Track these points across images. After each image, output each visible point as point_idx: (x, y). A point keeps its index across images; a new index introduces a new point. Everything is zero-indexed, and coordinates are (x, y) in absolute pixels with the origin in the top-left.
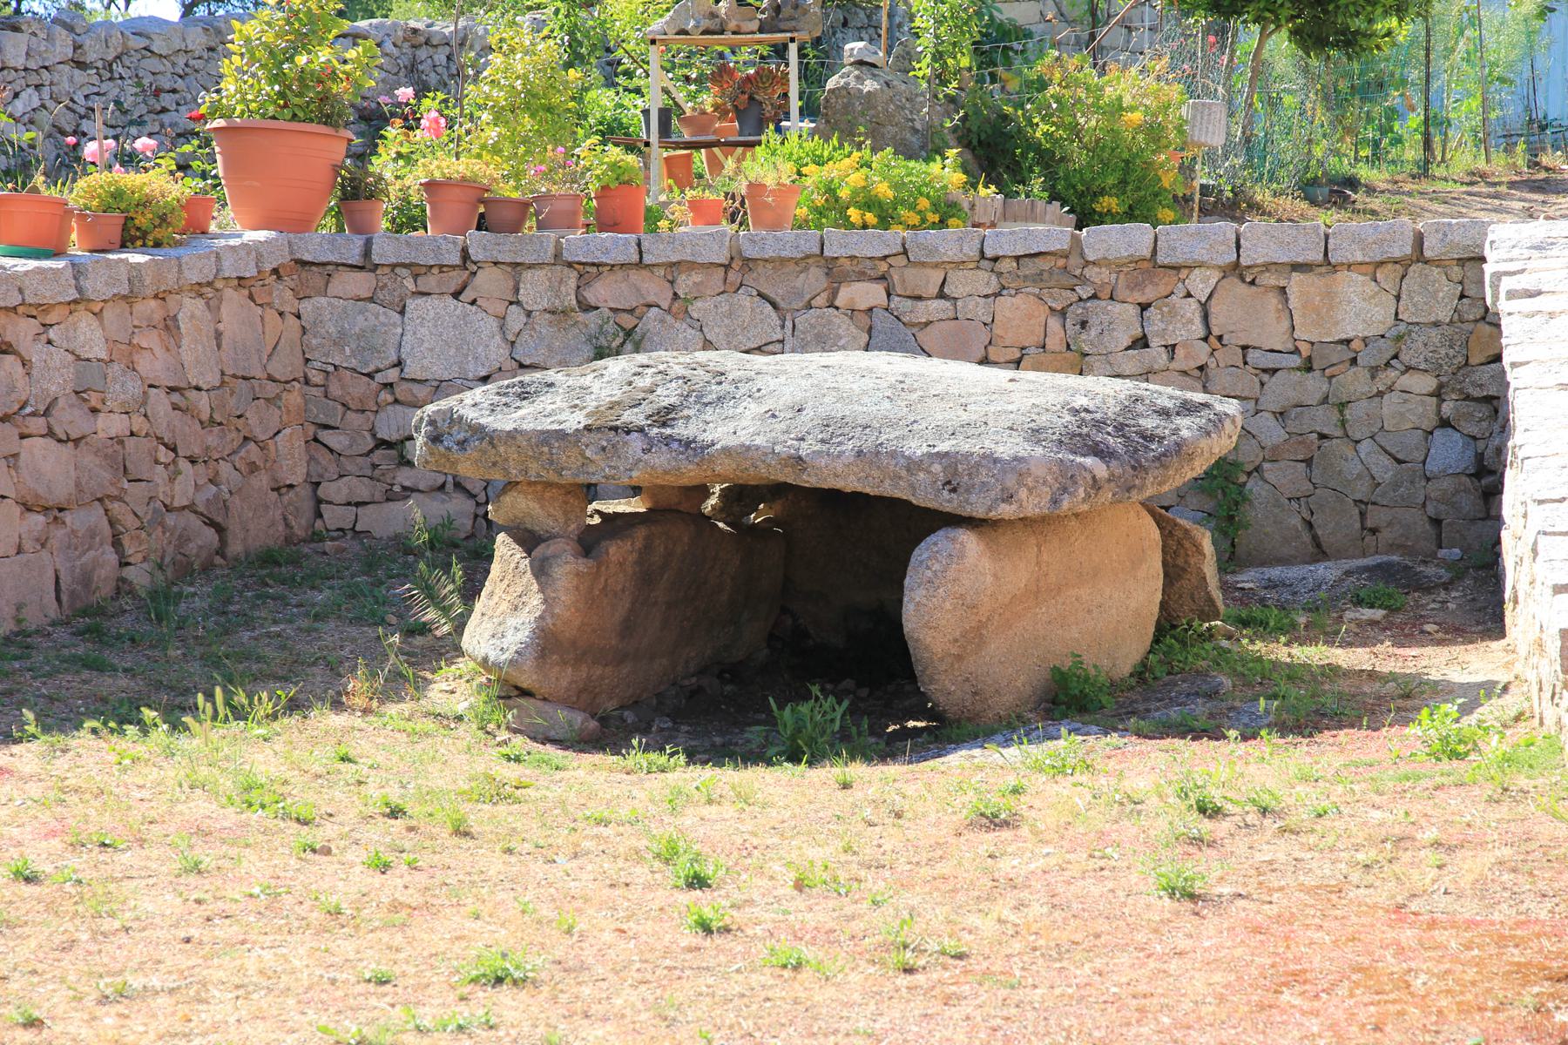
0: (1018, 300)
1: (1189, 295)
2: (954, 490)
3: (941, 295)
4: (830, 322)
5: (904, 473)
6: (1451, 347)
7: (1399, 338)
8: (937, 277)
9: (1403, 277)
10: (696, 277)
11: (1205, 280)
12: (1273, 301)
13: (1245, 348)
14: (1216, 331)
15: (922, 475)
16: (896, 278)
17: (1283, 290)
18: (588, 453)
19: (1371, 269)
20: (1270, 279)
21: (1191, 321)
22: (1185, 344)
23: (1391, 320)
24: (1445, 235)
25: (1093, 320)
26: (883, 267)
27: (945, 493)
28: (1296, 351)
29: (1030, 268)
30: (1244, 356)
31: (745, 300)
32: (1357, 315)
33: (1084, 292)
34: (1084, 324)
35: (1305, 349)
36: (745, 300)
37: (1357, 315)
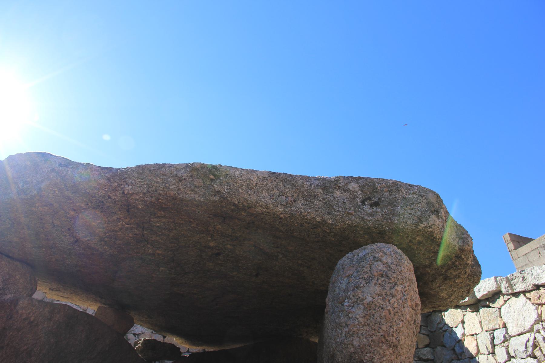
2: (376, 204)
5: (319, 191)
15: (338, 193)
27: (367, 208)
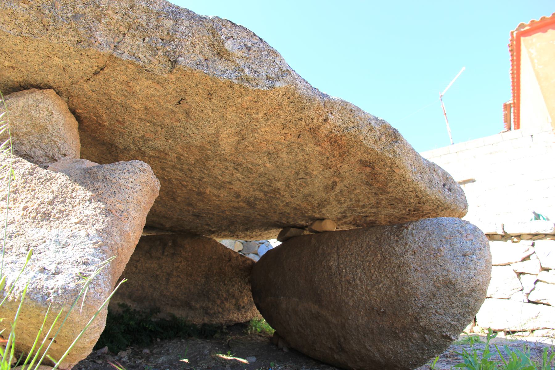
18: (229, 45)
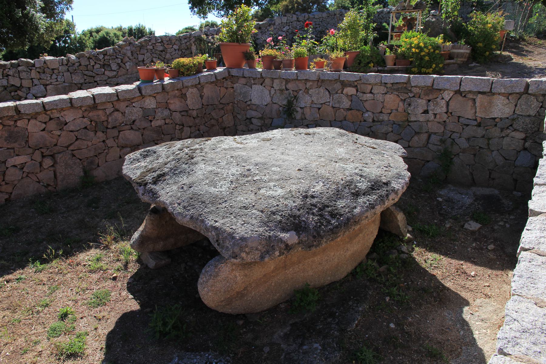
0: (391, 96)
1: (443, 99)
3: (371, 92)
4: (341, 98)
6: (533, 124)
7: (513, 120)
8: (370, 87)
9: (519, 98)
10: (311, 83)
11: (449, 94)
12: (470, 103)
13: (459, 117)
14: (450, 111)
16: (359, 87)
17: (474, 100)
19: (507, 95)
20: (471, 96)
21: (442, 107)
22: (440, 114)
23: (511, 113)
24: (539, 86)
25: (412, 104)
26: (356, 84)
28: (476, 120)
29: (395, 87)
30: (458, 119)
31: (322, 90)
32: (499, 110)
33: (411, 95)
34: (410, 105)
35: (479, 120)
36: (322, 90)
37: (499, 110)
